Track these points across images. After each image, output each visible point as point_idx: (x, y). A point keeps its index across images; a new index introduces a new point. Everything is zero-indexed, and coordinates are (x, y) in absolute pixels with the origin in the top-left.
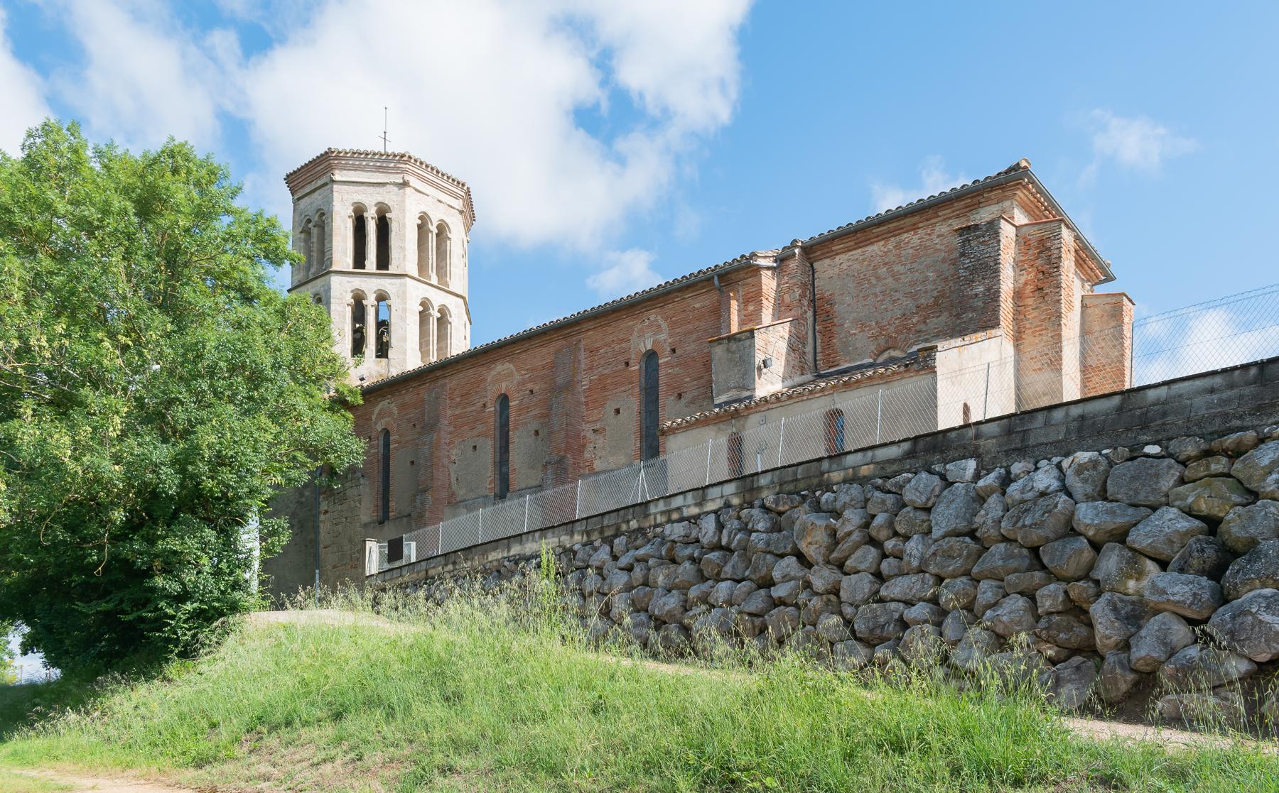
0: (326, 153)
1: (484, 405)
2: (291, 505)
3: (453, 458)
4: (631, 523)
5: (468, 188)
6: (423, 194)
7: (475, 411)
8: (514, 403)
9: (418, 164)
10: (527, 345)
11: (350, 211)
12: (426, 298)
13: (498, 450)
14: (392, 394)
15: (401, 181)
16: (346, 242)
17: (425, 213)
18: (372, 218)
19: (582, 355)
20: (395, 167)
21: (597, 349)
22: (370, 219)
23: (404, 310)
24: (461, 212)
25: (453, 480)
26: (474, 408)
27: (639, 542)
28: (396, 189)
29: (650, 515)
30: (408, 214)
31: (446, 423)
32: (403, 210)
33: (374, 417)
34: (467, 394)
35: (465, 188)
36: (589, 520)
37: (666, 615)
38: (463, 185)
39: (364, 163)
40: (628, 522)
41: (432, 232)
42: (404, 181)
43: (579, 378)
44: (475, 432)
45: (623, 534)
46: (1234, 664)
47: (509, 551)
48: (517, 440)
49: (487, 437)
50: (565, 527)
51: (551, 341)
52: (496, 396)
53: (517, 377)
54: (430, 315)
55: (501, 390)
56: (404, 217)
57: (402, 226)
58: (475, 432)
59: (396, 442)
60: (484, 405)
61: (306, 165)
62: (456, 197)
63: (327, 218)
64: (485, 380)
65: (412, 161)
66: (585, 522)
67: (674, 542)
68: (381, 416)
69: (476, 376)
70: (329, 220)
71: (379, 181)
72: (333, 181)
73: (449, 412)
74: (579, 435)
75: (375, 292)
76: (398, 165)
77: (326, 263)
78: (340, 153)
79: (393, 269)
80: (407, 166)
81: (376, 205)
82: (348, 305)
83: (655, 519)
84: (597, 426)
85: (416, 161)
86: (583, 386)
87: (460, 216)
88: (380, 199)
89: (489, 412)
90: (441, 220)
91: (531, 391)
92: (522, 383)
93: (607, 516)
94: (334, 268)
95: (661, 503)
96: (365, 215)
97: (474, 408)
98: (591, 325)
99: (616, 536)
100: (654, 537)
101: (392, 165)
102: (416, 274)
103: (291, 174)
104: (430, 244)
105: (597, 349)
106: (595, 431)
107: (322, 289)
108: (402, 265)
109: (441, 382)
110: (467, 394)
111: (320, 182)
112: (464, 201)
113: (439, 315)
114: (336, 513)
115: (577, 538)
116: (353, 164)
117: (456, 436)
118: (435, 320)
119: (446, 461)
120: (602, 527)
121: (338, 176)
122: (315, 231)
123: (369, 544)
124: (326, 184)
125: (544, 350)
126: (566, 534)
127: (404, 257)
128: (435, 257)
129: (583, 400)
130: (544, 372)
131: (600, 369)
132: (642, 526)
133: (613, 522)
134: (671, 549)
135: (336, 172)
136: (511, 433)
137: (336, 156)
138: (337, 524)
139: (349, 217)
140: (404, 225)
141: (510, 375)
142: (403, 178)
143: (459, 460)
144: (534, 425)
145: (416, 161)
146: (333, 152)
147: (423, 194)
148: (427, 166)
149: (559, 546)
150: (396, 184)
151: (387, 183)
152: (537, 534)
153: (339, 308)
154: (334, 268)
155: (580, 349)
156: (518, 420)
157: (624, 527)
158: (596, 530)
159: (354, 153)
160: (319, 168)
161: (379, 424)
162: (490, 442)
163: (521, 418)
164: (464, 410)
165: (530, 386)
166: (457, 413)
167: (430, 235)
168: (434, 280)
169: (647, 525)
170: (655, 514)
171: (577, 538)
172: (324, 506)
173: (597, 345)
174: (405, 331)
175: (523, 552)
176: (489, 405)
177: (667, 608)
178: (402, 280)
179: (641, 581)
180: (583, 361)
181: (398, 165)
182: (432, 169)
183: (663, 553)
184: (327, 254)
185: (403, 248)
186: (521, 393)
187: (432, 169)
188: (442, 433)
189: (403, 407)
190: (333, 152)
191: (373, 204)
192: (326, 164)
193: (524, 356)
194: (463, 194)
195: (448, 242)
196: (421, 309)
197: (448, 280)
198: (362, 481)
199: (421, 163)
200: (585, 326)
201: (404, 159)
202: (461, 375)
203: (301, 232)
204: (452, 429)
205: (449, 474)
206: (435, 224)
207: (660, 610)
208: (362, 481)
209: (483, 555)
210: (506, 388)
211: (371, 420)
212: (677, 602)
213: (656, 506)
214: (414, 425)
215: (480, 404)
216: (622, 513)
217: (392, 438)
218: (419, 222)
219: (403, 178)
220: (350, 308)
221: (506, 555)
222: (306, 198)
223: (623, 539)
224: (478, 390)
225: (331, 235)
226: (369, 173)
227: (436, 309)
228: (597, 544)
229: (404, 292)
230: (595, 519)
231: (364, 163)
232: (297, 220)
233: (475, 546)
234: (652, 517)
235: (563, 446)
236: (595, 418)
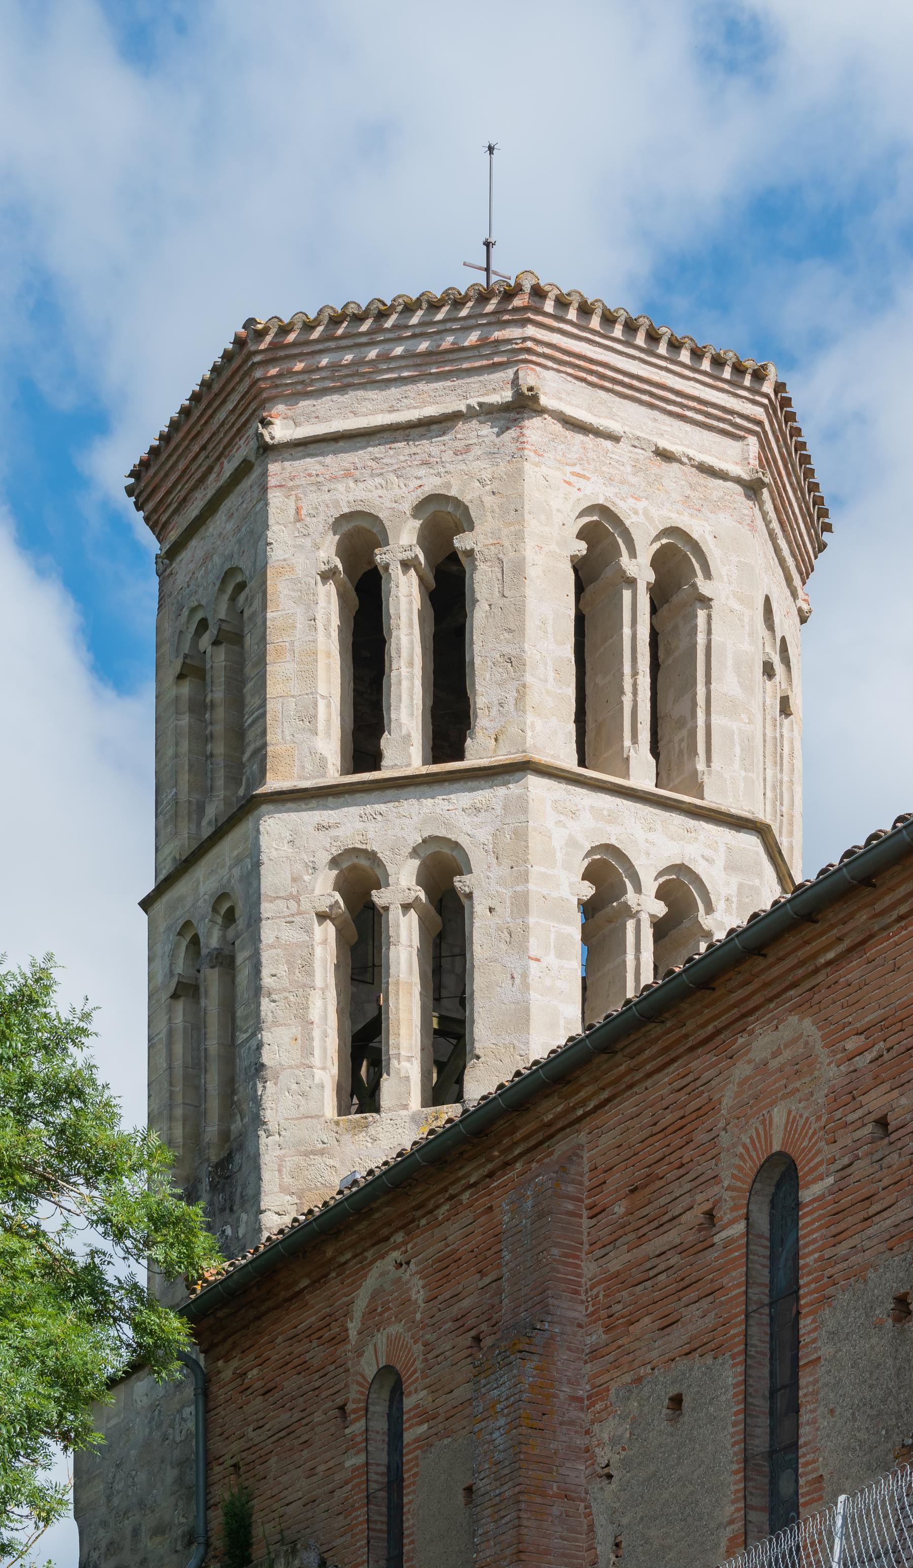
0: (239, 342)
1: (710, 1215)
3: (603, 1455)
7: (680, 1249)
8: (816, 1189)
9: (572, 315)
10: (863, 917)
12: (609, 848)
13: (761, 1404)
15: (507, 395)
16: (314, 678)
17: (603, 510)
20: (483, 343)
22: (396, 570)
23: (521, 904)
24: (752, 489)
26: (673, 1236)
28: (487, 431)
30: (532, 525)
31: (579, 1312)
33: (353, 1327)
34: (650, 1178)
35: (768, 387)
39: (373, 354)
41: (631, 582)
44: (678, 1337)
46: (496, 1153)
48: (826, 1351)
52: (750, 1167)
54: (627, 912)
55: (768, 1137)
56: (519, 536)
58: (678, 1337)
59: (425, 1416)
60: (710, 1215)
63: (249, 601)
69: (683, 1097)
70: (257, 603)
71: (431, 411)
72: (267, 450)
73: (589, 1269)
75: (415, 853)
76: (498, 335)
77: (247, 771)
78: (284, 330)
81: (418, 509)
82: (322, 917)
85: (562, 303)
87: (746, 506)
88: (432, 484)
89: (729, 1242)
90: (672, 531)
91: (882, 1123)
94: (274, 783)
96: (380, 557)
97: (673, 1236)
101: (473, 338)
102: (568, 760)
103: (144, 464)
104: (627, 631)
107: (236, 872)
108: (513, 730)
109: (561, 1147)
110: (650, 1178)
111: (228, 468)
112: (764, 445)
113: (660, 909)
117: (616, 1364)
118: (647, 934)
122: (218, 660)
124: (245, 468)
127: (522, 692)
128: (645, 681)
136: (805, 1323)
137: (273, 347)
139: (325, 576)
140: (519, 569)
142: (515, 382)
145: (562, 303)
146: (260, 335)
150: (487, 412)
151: (456, 416)
153: (290, 935)
154: (274, 783)
159: (335, 321)
160: (222, 415)
161: (369, 1351)
163: (843, 1249)
164: (639, 1253)
167: (627, 594)
174: (526, 986)
176: (724, 1214)
178: (514, 789)
181: (498, 335)
186: (845, 1139)
190: (260, 335)
191: (407, 507)
193: (853, 971)
194: (759, 413)
195: (701, 614)
196: (588, 890)
197: (701, 766)
201: (517, 302)
202: (628, 1105)
203: (181, 677)
204: (597, 1336)
205: (591, 1528)
206: (646, 551)
210: (790, 1123)
211: (345, 1340)
214: (477, 1339)
215: (695, 1216)
217: (408, 1402)
218: (582, 547)
219: (515, 382)
222: (193, 543)
224: (687, 1154)
225: (262, 661)
226: (394, 392)
227: (650, 886)
229: (520, 835)
231: (373, 354)
232: (168, 634)
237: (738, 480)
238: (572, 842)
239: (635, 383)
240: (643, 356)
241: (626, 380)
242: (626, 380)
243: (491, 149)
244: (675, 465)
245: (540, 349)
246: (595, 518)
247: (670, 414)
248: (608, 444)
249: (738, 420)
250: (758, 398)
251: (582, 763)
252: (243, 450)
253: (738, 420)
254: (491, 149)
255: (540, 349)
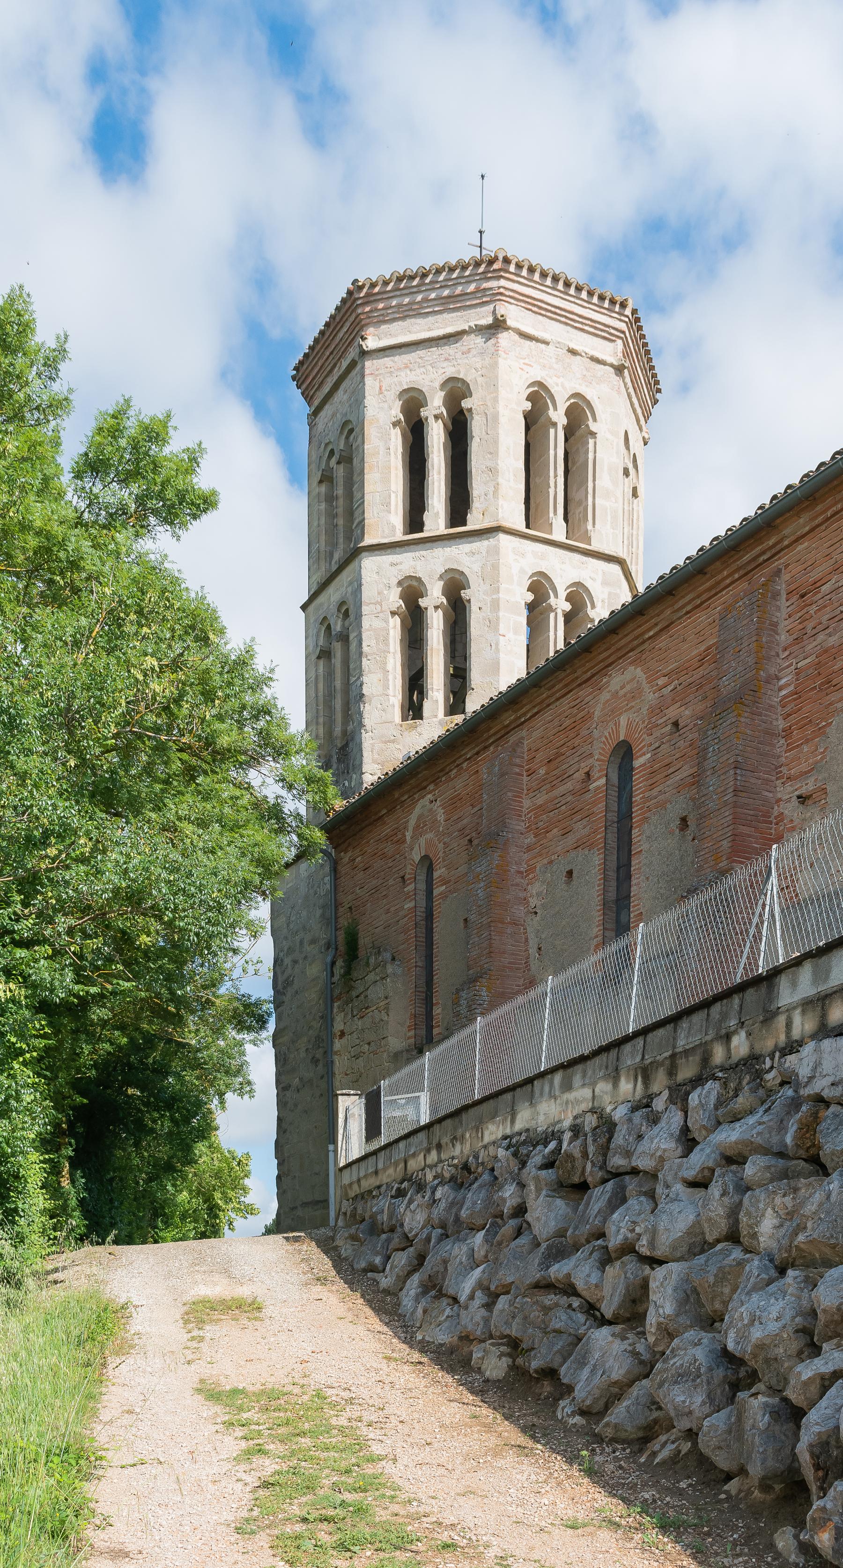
0: (350, 293)
1: (588, 774)
2: (314, 1023)
3: (533, 902)
4: (735, 1041)
5: (634, 311)
6: (537, 340)
7: (572, 793)
9: (524, 272)
11: (396, 412)
13: (612, 874)
14: (435, 781)
15: (489, 320)
16: (389, 481)
17: (540, 384)
18: (436, 417)
19: (784, 606)
20: (478, 290)
21: (816, 585)
23: (495, 605)
24: (619, 370)
25: (533, 951)
27: (742, 1101)
29: (777, 1012)
30: (503, 393)
31: (521, 827)
32: (493, 386)
34: (558, 755)
35: (628, 312)
36: (650, 1036)
37: (755, 1356)
38: (623, 305)
39: (419, 298)
40: (727, 1038)
41: (555, 425)
42: (496, 319)
43: (773, 670)
44: (571, 840)
45: (715, 1078)
47: (513, 1122)
48: (645, 846)
49: (591, 846)
50: (604, 1056)
51: (716, 590)
52: (609, 749)
53: (650, 697)
54: (550, 609)
56: (496, 400)
57: (492, 420)
58: (571, 840)
59: (445, 882)
60: (588, 774)
61: (322, 333)
62: (606, 334)
64: (589, 716)
65: (512, 268)
66: (640, 1041)
67: (820, 1100)
68: (419, 830)
69: (575, 711)
70: (359, 440)
71: (450, 330)
73: (527, 803)
74: (767, 815)
75: (441, 577)
78: (373, 285)
79: (475, 521)
80: (502, 282)
81: (443, 385)
82: (393, 613)
83: (789, 1025)
84: (808, 786)
85: (519, 266)
86: (780, 689)
88: (450, 372)
89: (598, 788)
91: (676, 724)
92: (659, 709)
93: (684, 1024)
95: (806, 972)
96: (424, 413)
98: (802, 523)
99: (698, 1081)
100: (782, 1084)
101: (472, 287)
104: (552, 452)
105: (816, 585)
106: (803, 799)
109: (513, 738)
110: (558, 755)
111: (345, 364)
112: (626, 345)
113: (568, 607)
114: (355, 1035)
115: (626, 1086)
116: (399, 305)
119: (520, 911)
120: (673, 1056)
121: (371, 343)
123: (343, 1103)
124: (353, 364)
125: (702, 618)
126: (605, 1078)
129: (781, 724)
130: (701, 672)
131: (821, 637)
132: (758, 1050)
133: (695, 1040)
134: (809, 1127)
135: (370, 331)
136: (635, 832)
137: (368, 295)
138: (356, 1057)
139: (395, 425)
141: (636, 694)
143: (543, 906)
144: (677, 808)
145: (519, 266)
146: (361, 288)
147: (537, 340)
148: (544, 275)
149: (593, 1111)
150: (480, 330)
151: (463, 333)
152: (558, 1078)
153: (377, 624)
154: (368, 541)
155: (776, 595)
156: (650, 799)
157: (719, 1055)
158: (662, 1064)
160: (341, 335)
162: (597, 859)
163: (655, 792)
165: (673, 712)
166: (540, 802)
167: (552, 431)
168: (559, 532)
169: (769, 1044)
170: (790, 1010)
171: (626, 1086)
172: (338, 1026)
173: (815, 575)
174: (497, 650)
175: (533, 1124)
176: (595, 774)
177: (757, 1333)
179: (723, 1226)
180: (784, 625)
182: (556, 279)
183: (789, 1139)
184: (356, 514)
185: (493, 471)
186: (657, 733)
187: (556, 279)
188: (513, 850)
189: (453, 805)
190: (361, 288)
191: (437, 385)
192: (354, 316)
193: (663, 642)
194: (623, 326)
195: (591, 441)
196: (530, 597)
197: (590, 527)
198: (390, 969)
199: (531, 270)
200: (790, 530)
201: (496, 266)
202: (547, 715)
203: (321, 482)
204: (530, 839)
205: (527, 940)
206: (562, 407)
207: (742, 1337)
208: (390, 969)
209: (477, 1131)
211: (404, 841)
212: (789, 1314)
213: (794, 984)
214: (470, 841)
216: (716, 1009)
217: (436, 875)
220: (397, 620)
221: (508, 1131)
223: (712, 1089)
224: (577, 742)
225: (362, 473)
226: (431, 319)
227: (562, 594)
228: (659, 1104)
229: (495, 567)
230: (661, 1032)
231: (419, 298)
233: (466, 1108)
234: (782, 1020)
235: (725, 844)
236: (804, 767)
237: (612, 365)
238: (522, 571)
239: (558, 311)
240: (562, 295)
241: (553, 309)
242: (553, 309)
243: (483, 177)
244: (578, 357)
245: (507, 293)
246: (536, 389)
247: (576, 328)
248: (543, 346)
249: (612, 331)
250: (623, 318)
251: (528, 526)
252: (352, 354)
253: (612, 331)
254: (483, 177)
255: (507, 293)
